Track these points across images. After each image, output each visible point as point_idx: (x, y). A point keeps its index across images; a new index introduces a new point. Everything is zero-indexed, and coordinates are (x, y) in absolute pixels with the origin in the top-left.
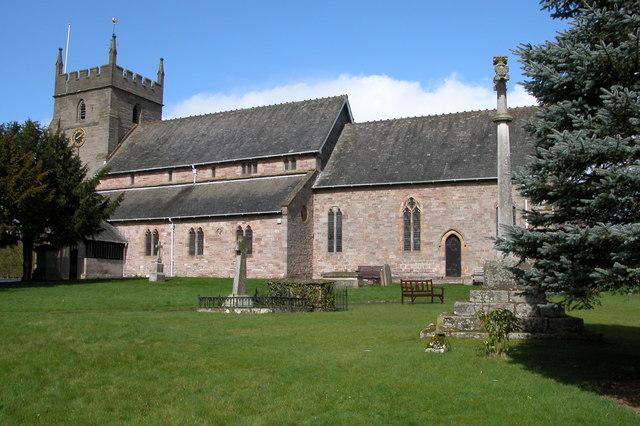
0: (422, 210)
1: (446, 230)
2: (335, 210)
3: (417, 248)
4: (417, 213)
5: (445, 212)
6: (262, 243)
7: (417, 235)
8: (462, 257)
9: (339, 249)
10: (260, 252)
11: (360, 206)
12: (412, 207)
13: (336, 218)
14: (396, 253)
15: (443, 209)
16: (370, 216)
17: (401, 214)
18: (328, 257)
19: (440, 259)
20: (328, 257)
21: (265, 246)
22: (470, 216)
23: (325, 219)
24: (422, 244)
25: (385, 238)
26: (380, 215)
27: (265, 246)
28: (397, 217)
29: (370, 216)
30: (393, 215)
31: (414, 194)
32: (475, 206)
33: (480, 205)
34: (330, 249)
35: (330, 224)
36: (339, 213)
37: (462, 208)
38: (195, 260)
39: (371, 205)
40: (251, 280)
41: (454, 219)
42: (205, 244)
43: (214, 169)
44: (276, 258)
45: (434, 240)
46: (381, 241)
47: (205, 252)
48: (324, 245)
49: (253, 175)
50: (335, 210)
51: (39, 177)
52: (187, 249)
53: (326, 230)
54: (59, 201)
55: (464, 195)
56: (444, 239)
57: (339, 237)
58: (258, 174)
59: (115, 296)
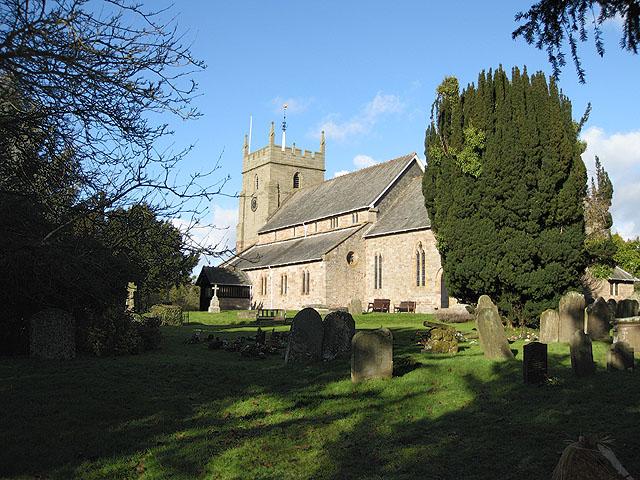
13: (379, 259)
17: (414, 255)
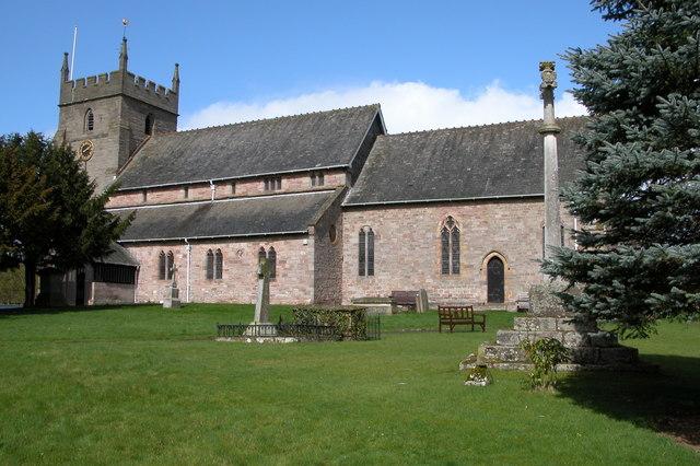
0: (461, 229)
1: (488, 251)
2: (366, 230)
3: (456, 271)
4: (456, 233)
5: (487, 232)
6: (287, 266)
7: (456, 257)
8: (506, 281)
9: (371, 272)
10: (285, 275)
11: (394, 226)
12: (450, 227)
13: (367, 239)
14: (433, 277)
15: (485, 228)
16: (405, 236)
17: (439, 234)
18: (359, 282)
19: (481, 283)
20: (359, 282)
21: (290, 269)
22: (514, 236)
23: (356, 240)
24: (461, 267)
25: (421, 260)
26: (415, 235)
27: (290, 269)
28: (435, 237)
29: (405, 236)
30: (430, 235)
31: (452, 212)
32: (520, 225)
33: (525, 224)
34: (361, 273)
35: (361, 245)
36: (371, 233)
37: (505, 228)
38: (214, 285)
39: (405, 224)
40: (275, 307)
41: (496, 239)
42: (224, 267)
43: (234, 185)
44: (301, 282)
45: (475, 263)
46: (416, 263)
47: (225, 276)
48: (355, 268)
49: (277, 191)
50: (366, 230)
51: (43, 194)
52: (205, 272)
53: (356, 251)
54: (64, 219)
55: (507, 213)
56: (486, 261)
57: (371, 259)
58: (283, 190)
59: (126, 324)
